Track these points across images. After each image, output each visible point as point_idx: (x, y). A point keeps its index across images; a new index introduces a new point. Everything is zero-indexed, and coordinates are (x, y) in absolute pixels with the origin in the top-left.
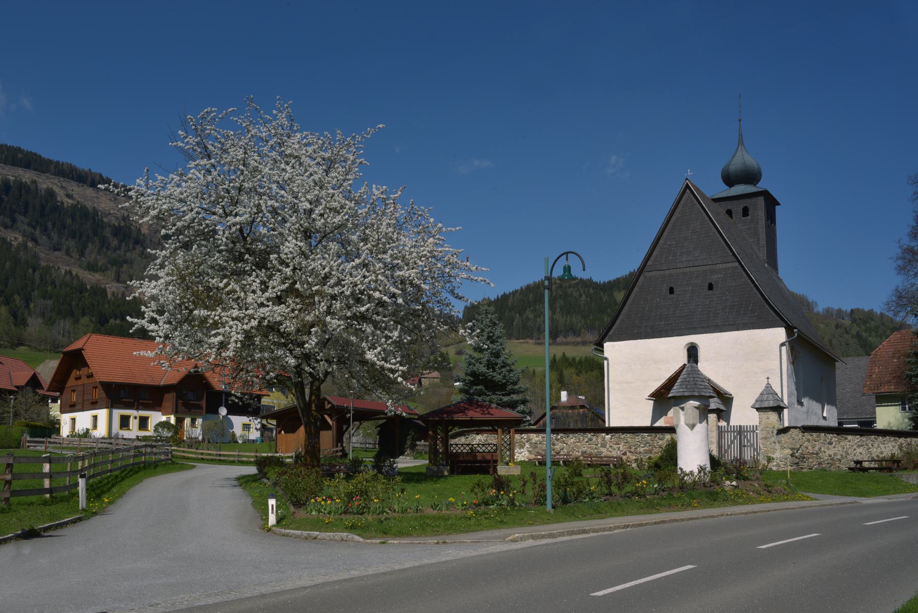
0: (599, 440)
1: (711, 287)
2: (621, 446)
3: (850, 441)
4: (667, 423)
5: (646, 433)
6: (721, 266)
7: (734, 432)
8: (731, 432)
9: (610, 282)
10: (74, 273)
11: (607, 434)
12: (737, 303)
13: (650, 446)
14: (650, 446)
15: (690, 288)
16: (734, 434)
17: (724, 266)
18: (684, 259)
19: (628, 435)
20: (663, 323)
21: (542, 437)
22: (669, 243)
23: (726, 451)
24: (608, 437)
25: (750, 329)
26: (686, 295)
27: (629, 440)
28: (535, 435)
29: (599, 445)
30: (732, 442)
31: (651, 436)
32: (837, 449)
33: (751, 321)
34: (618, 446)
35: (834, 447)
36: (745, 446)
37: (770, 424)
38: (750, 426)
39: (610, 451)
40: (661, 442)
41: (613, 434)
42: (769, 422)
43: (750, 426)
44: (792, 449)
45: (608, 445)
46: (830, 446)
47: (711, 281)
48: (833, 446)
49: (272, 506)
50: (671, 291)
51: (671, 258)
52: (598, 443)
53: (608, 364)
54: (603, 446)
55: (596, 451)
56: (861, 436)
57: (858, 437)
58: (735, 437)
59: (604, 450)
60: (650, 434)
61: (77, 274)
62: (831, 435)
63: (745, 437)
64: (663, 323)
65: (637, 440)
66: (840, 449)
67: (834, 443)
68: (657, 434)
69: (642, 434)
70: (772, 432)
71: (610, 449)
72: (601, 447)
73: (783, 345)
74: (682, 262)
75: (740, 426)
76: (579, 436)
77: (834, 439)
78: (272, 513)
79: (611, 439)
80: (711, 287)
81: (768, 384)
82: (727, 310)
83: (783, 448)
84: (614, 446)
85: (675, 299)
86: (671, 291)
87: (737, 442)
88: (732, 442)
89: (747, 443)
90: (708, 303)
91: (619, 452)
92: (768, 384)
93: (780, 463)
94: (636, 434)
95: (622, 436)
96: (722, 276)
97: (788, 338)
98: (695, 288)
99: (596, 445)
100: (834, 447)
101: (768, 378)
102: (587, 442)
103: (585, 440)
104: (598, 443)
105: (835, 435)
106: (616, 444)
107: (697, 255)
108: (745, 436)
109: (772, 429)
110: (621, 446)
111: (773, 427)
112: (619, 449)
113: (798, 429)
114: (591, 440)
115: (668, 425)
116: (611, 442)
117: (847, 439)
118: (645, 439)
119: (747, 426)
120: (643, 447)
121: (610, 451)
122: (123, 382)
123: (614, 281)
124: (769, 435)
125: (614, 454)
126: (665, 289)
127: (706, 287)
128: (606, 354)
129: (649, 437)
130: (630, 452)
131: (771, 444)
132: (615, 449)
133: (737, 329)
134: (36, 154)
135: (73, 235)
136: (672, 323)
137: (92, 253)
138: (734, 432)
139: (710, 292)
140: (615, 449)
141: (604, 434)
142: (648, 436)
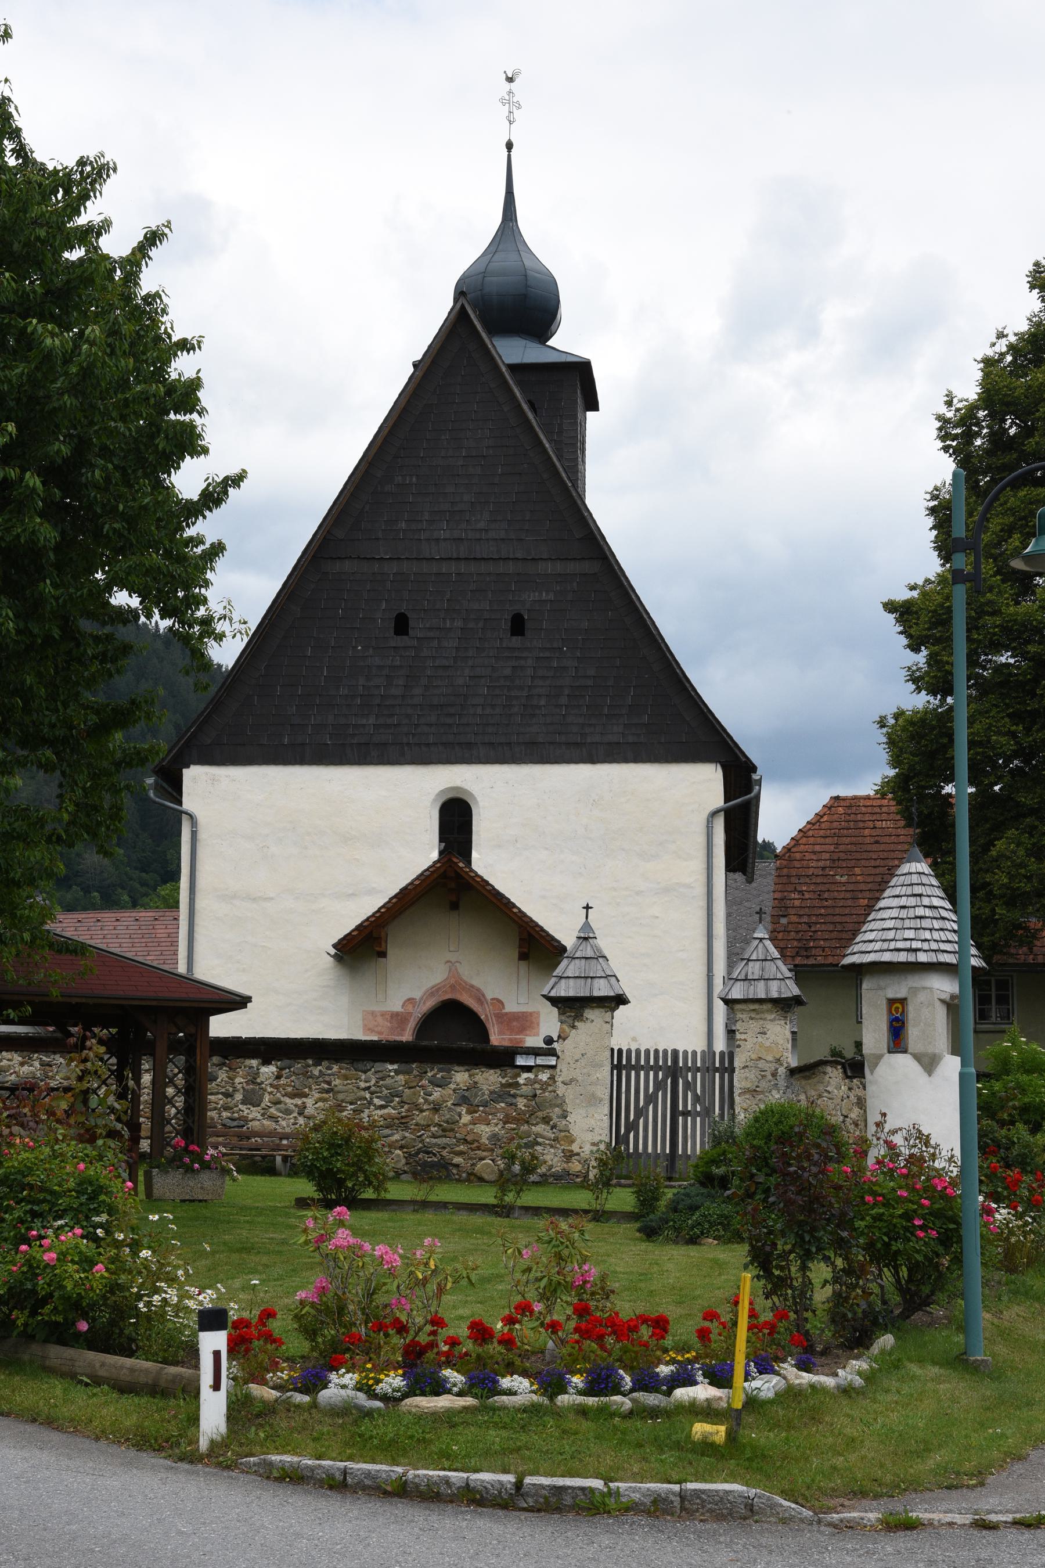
0: (238, 1080)
1: (518, 626)
2: (309, 1102)
4: (371, 1031)
5: (392, 1063)
6: (549, 568)
7: (656, 1068)
8: (647, 1068)
11: (266, 1062)
12: (590, 683)
13: (402, 1103)
14: (402, 1103)
15: (458, 624)
16: (656, 1076)
17: (559, 567)
19: (335, 1068)
20: (372, 720)
22: (399, 479)
24: (268, 1071)
25: (626, 760)
27: (337, 1082)
28: (17, 1058)
29: (239, 1097)
30: (651, 1099)
31: (408, 1072)
33: (631, 739)
34: (299, 1102)
36: (686, 1114)
37: (768, 1049)
39: (271, 1117)
40: (437, 1094)
41: (287, 1062)
42: (768, 1044)
43: (629, 1051)
49: (217, 1354)
50: (401, 625)
51: (404, 525)
52: (235, 1090)
53: (194, 835)
54: (252, 1099)
55: (225, 1114)
58: (659, 1085)
59: (254, 1113)
60: (404, 1067)
63: (688, 1086)
64: (372, 720)
65: (363, 1085)
69: (378, 1066)
70: (774, 1074)
71: (273, 1111)
72: (243, 1103)
73: (714, 814)
75: (675, 1053)
78: (216, 1387)
79: (278, 1077)
80: (518, 626)
81: (587, 926)
82: (564, 700)
84: (287, 1100)
86: (401, 625)
87: (664, 1101)
88: (651, 1099)
89: (694, 1105)
90: (508, 672)
91: (301, 1121)
92: (587, 926)
94: (360, 1066)
96: (551, 596)
97: (726, 801)
98: (471, 625)
99: (227, 1095)
101: (587, 908)
104: (235, 1090)
106: (292, 1096)
107: (482, 525)
108: (688, 1086)
109: (773, 1066)
110: (309, 1102)
111: (778, 1061)
112: (301, 1111)
115: (375, 1038)
116: (276, 1087)
118: (388, 1081)
119: (685, 1052)
120: (382, 1107)
121: (271, 1117)
124: (764, 1084)
125: (285, 1125)
127: (506, 625)
128: (189, 803)
129: (401, 1077)
132: (287, 1112)
133: (591, 758)
136: (398, 725)
138: (656, 1068)
139: (516, 641)
140: (287, 1112)
141: (254, 1062)
142: (397, 1072)
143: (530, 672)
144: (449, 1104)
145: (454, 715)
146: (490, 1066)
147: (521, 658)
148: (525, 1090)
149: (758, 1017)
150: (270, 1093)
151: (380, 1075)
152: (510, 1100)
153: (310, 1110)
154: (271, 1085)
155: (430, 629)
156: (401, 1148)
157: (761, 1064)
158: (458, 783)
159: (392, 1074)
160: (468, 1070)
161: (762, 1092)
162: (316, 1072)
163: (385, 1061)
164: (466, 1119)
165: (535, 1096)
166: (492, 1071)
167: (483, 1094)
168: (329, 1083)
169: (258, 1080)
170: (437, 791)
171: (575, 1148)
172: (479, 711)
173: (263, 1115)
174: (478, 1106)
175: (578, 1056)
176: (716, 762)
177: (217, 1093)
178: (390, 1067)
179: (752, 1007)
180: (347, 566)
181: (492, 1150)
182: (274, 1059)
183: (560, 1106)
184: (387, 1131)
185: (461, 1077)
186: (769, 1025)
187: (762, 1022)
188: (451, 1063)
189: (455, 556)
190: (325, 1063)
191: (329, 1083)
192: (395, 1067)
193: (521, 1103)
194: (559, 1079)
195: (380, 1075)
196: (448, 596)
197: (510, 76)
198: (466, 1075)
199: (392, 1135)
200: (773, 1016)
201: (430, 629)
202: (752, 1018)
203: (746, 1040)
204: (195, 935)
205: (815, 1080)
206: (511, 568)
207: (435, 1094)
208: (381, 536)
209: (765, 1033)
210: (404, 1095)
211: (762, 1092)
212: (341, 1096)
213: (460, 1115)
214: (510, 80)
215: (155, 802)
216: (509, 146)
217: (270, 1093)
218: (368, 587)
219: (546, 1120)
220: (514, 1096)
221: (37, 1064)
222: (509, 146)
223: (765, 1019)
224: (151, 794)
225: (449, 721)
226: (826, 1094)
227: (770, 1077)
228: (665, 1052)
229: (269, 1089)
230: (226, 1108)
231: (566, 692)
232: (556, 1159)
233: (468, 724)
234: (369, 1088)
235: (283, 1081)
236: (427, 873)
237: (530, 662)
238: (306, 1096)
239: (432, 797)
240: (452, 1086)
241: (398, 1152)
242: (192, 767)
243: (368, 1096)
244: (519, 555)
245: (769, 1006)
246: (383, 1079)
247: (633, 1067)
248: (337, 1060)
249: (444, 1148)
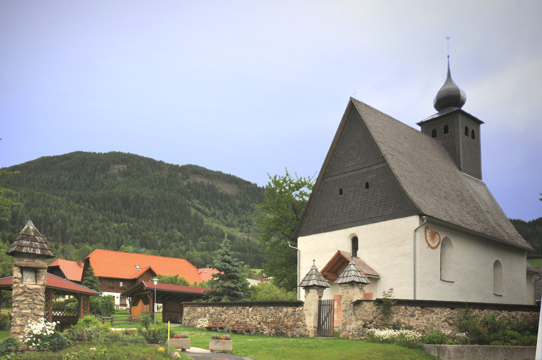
1: (367, 186)
3: (437, 314)
5: (272, 306)
9: (533, 221)
10: (220, 228)
11: (250, 307)
15: (353, 189)
17: (377, 167)
18: (349, 165)
19: (262, 308)
21: (216, 309)
22: (340, 153)
23: (323, 324)
25: (393, 219)
26: (350, 195)
29: (245, 316)
32: (420, 321)
34: (256, 317)
35: (417, 319)
37: (349, 298)
38: (325, 300)
42: (349, 296)
43: (327, 300)
44: (364, 320)
45: (250, 316)
46: (411, 319)
47: (367, 181)
48: (415, 318)
50: (341, 192)
55: (243, 320)
56: (452, 309)
57: (448, 310)
60: (274, 307)
61: (221, 229)
62: (413, 308)
65: (267, 312)
66: (424, 321)
67: (417, 316)
68: (279, 307)
69: (270, 307)
72: (247, 318)
74: (348, 167)
76: (234, 308)
77: (417, 312)
79: (252, 311)
80: (367, 186)
82: (378, 205)
83: (357, 320)
84: (254, 317)
85: (343, 199)
86: (341, 192)
90: (365, 199)
93: (355, 333)
95: (259, 309)
96: (375, 176)
100: (417, 319)
101: (314, 261)
102: (239, 313)
103: (238, 312)
104: (245, 314)
105: (418, 308)
107: (358, 160)
110: (258, 317)
113: (372, 302)
114: (241, 312)
117: (433, 312)
118: (271, 311)
120: (271, 318)
122: (112, 277)
123: (537, 220)
126: (337, 192)
127: (364, 186)
130: (263, 322)
131: (349, 316)
133: (385, 220)
134: (204, 168)
135: (220, 209)
137: (230, 217)
141: (248, 307)
143: (370, 198)
144: (283, 317)
145: (352, 214)
146: (291, 306)
147: (368, 195)
148: (297, 312)
149: (346, 288)
150: (251, 315)
151: (270, 310)
152: (294, 315)
153: (258, 319)
154: (251, 313)
155: (347, 192)
156: (274, 328)
157: (347, 302)
158: (353, 232)
159: (272, 309)
160: (286, 308)
161: (347, 311)
162: (259, 310)
163: (271, 306)
164: (286, 320)
165: (299, 314)
166: (291, 308)
167: (289, 314)
168: (261, 312)
169: (249, 312)
170: (350, 234)
171: (307, 328)
172: (358, 211)
173: (250, 320)
174: (288, 317)
175: (308, 303)
176: (417, 215)
177: (242, 315)
178: (272, 307)
179: (344, 285)
180: (329, 179)
181: (291, 329)
182: (251, 307)
183: (304, 316)
184: (271, 324)
185: (285, 309)
186: (349, 290)
187: (347, 290)
188: (283, 306)
189: (352, 170)
190: (260, 307)
191: (261, 312)
192: (273, 307)
193: (297, 316)
194: (304, 309)
195: (270, 310)
196: (351, 182)
197: (448, 37)
198: (286, 309)
199: (272, 325)
200: (350, 287)
201: (347, 192)
202: (345, 289)
203: (343, 295)
204: (300, 277)
205: (360, 306)
206: (365, 170)
207: (280, 314)
208: (336, 169)
209: (348, 293)
210: (274, 315)
211: (347, 311)
212: (263, 315)
213: (285, 320)
214: (448, 38)
215: (291, 247)
216: (448, 57)
217: (251, 315)
218: (334, 184)
219: (301, 321)
220: (295, 314)
221: (214, 309)
222: (448, 57)
223: (348, 289)
224: (290, 246)
225: (351, 216)
226: (363, 310)
227: (349, 306)
228: (327, 300)
229: (251, 314)
230: (244, 319)
231: (379, 202)
232: (303, 331)
233: (355, 216)
234: (268, 313)
235: (253, 312)
236: (334, 257)
237: (370, 196)
238: (257, 316)
239: (347, 237)
240: (283, 312)
241: (274, 329)
242: (299, 237)
243: (268, 315)
244: (367, 166)
245: (347, 285)
246: (270, 311)
247: (328, 305)
248: (262, 306)
249: (282, 328)
